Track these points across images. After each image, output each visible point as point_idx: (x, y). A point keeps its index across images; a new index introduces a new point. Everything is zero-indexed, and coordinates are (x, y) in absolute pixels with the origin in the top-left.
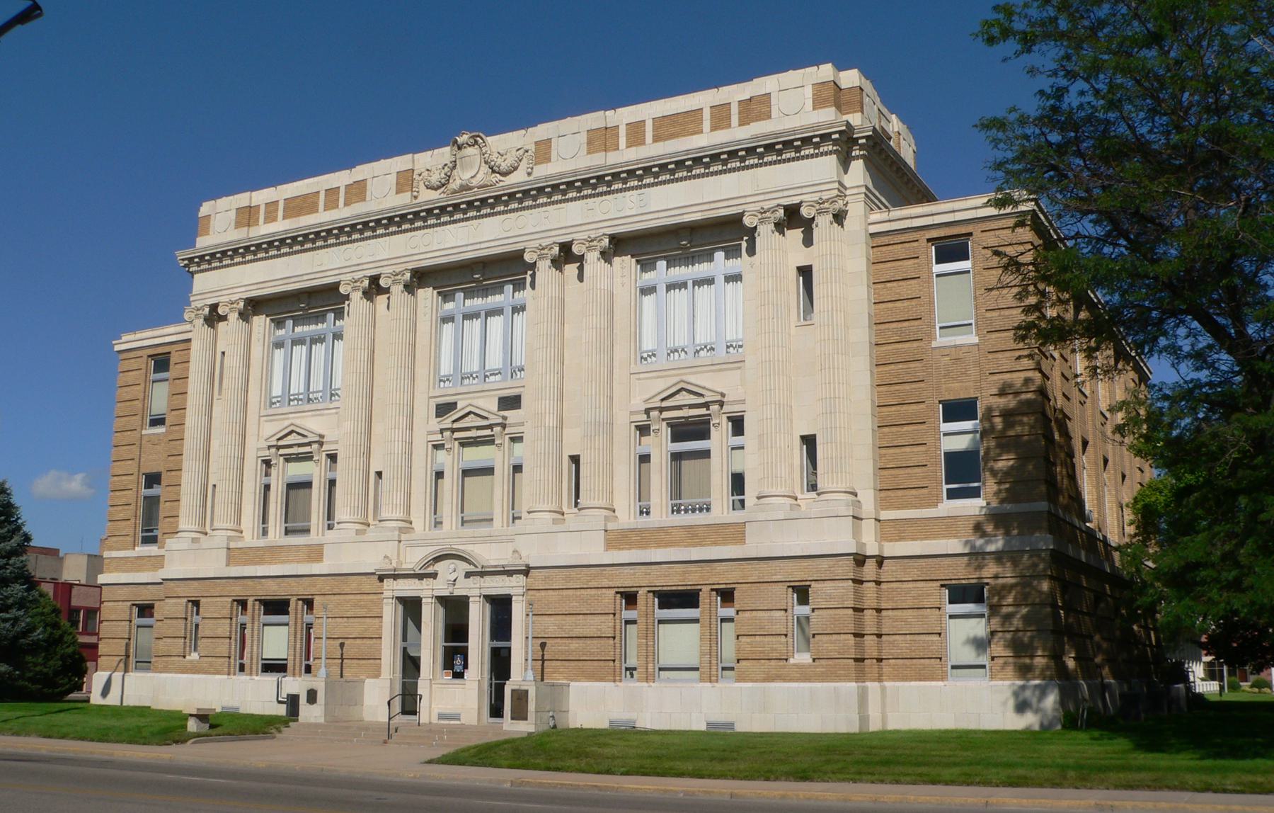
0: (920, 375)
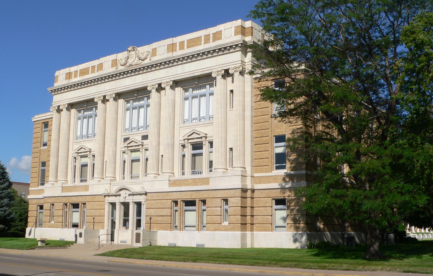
0: (268, 127)
